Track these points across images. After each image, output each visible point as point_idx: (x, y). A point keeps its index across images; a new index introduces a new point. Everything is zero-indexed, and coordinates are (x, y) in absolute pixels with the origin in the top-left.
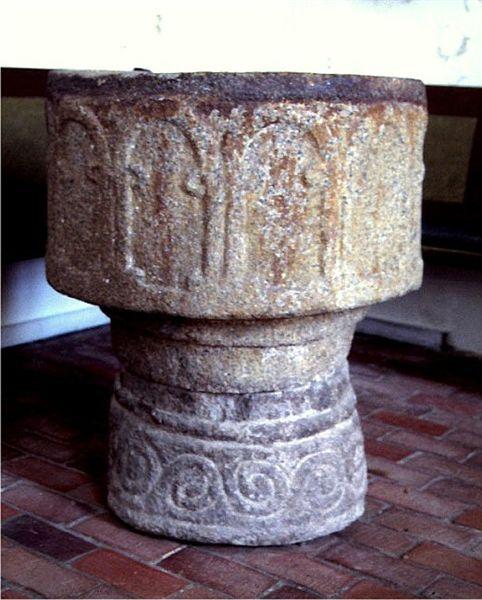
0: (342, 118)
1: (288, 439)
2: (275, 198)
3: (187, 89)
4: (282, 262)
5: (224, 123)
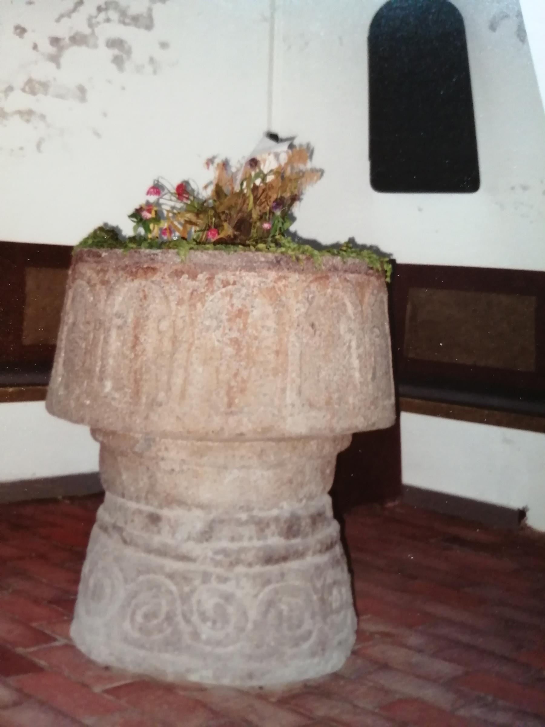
0: (290, 283)
1: (250, 565)
2: (231, 340)
3: (165, 260)
4: (235, 389)
5: (191, 284)
